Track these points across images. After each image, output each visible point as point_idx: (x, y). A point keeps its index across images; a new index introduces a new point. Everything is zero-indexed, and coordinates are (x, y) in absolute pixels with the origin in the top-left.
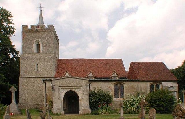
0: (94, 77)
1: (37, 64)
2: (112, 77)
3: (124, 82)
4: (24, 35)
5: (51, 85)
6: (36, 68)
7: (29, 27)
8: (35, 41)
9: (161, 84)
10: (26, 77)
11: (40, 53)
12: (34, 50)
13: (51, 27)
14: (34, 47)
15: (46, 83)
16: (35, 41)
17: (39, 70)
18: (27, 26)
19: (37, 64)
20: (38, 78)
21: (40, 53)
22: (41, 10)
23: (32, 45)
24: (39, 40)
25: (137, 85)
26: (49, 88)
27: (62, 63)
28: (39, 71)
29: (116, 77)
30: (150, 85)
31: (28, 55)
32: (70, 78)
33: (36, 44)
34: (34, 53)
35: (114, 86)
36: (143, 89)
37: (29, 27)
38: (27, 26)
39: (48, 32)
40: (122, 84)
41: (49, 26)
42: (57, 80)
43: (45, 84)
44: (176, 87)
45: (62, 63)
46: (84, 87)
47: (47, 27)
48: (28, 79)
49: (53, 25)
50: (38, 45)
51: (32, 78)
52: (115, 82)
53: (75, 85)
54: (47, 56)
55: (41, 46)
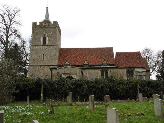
0: (88, 64)
1: (44, 54)
2: (102, 64)
3: (108, 69)
4: (34, 30)
5: (56, 73)
6: (42, 57)
7: (38, 24)
8: (42, 35)
9: (134, 70)
10: (34, 65)
11: (46, 45)
12: (41, 42)
13: (56, 23)
14: (42, 39)
15: (52, 71)
16: (42, 35)
17: (45, 59)
18: (36, 23)
19: (44, 54)
20: (43, 66)
21: (46, 45)
22: (47, 7)
23: (40, 38)
24: (46, 34)
25: (117, 71)
26: (55, 74)
27: (64, 52)
28: (45, 60)
29: (106, 64)
30: (127, 71)
31: (37, 47)
32: (69, 68)
33: (43, 37)
34: (41, 45)
35: (101, 72)
36: (121, 74)
37: (38, 24)
38: (36, 23)
39: (53, 27)
40: (106, 71)
41: (54, 22)
42: (61, 69)
43: (51, 71)
44: (144, 72)
45: (64, 52)
46: (78, 73)
47: (52, 23)
48: (35, 67)
49: (57, 22)
50: (45, 38)
51: (39, 66)
52: (102, 69)
53: (72, 72)
54: (52, 47)
55: (47, 38)
